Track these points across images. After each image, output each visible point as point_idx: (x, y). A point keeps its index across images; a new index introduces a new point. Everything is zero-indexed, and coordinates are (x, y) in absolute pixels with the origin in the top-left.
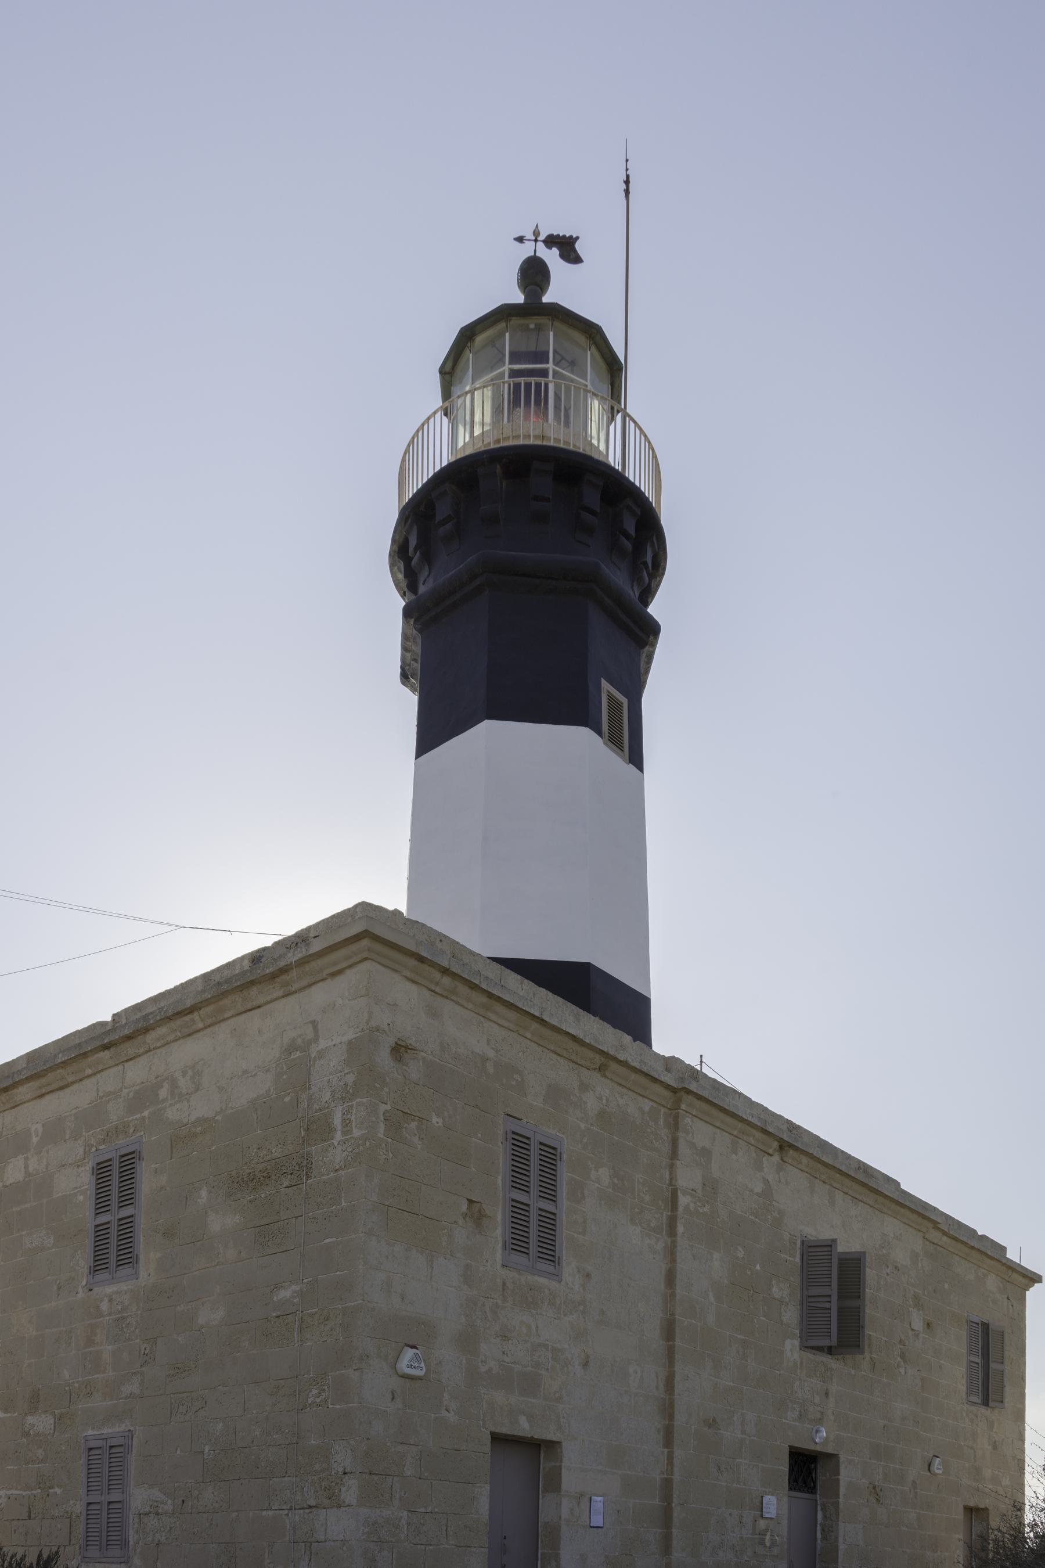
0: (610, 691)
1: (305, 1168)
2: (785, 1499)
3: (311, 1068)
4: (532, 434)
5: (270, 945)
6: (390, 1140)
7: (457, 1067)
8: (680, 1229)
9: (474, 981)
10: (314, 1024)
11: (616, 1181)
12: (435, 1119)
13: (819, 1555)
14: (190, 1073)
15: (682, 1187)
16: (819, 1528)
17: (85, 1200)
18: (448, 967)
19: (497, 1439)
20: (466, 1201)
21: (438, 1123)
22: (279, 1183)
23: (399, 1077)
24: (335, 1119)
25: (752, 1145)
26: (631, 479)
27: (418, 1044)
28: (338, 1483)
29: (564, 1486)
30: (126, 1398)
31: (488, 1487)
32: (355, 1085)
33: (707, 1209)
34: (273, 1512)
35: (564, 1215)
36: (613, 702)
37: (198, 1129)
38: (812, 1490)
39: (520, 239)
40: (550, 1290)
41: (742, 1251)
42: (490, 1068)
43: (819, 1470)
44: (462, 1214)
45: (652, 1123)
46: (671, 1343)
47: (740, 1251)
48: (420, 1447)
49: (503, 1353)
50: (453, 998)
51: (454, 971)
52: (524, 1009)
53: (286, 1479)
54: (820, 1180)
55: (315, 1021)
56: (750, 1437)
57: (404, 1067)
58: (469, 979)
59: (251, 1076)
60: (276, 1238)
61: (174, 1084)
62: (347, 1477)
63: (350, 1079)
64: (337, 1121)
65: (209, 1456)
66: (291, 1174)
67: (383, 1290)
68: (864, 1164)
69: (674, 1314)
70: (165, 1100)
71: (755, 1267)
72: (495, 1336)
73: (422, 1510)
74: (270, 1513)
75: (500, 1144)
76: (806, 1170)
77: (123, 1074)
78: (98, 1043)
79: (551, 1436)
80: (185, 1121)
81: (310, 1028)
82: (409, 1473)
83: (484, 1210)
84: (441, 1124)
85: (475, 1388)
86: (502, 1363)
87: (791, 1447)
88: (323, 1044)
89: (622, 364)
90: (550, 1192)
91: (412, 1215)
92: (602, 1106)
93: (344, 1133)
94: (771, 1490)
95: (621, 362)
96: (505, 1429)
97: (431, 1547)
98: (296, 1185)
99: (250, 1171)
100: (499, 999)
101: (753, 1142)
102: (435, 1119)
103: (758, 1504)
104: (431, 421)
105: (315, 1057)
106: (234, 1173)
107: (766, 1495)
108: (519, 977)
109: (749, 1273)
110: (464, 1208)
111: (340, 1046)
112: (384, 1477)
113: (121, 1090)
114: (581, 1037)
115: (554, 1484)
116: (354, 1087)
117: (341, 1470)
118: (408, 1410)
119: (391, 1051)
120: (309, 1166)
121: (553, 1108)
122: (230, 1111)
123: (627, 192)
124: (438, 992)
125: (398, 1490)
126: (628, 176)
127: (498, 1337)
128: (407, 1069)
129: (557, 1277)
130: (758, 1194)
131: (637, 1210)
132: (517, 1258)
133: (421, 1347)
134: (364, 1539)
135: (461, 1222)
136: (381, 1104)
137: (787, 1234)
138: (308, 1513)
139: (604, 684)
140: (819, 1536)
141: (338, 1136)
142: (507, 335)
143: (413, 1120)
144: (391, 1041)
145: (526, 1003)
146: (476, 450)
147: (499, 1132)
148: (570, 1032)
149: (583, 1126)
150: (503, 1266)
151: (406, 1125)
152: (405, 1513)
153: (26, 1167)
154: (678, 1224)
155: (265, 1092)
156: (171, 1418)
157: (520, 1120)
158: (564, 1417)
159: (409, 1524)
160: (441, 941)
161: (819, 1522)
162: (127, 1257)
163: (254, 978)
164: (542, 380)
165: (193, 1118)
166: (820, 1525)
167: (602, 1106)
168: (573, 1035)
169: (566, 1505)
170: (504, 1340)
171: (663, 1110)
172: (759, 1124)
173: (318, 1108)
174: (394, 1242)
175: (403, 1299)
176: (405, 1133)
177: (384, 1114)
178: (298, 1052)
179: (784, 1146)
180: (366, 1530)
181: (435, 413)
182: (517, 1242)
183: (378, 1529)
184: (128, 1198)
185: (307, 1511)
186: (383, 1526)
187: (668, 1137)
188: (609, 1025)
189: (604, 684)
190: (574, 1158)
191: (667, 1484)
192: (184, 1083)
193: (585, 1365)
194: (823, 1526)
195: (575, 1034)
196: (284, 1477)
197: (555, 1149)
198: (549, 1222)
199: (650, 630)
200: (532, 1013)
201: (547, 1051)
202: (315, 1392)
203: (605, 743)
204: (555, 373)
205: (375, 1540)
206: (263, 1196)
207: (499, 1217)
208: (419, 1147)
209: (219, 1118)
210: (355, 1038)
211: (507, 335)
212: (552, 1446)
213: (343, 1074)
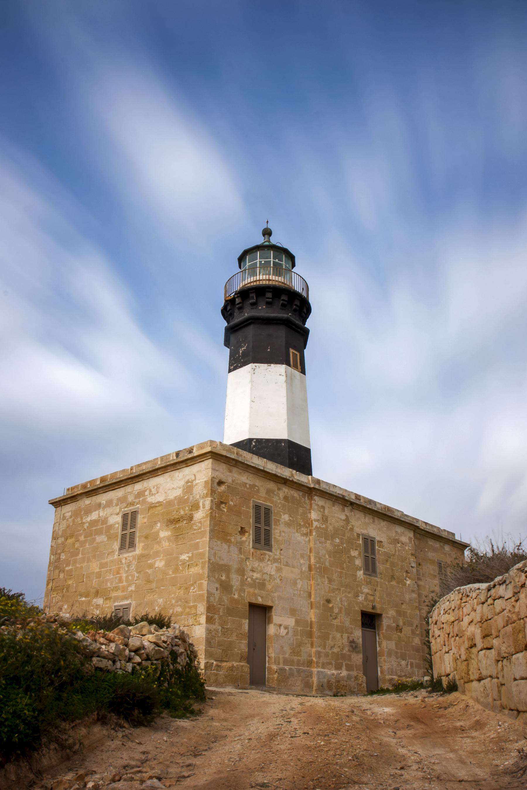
1: (191, 518)
10: (195, 475)
14: (156, 487)
16: (377, 643)
17: (119, 527)
26: (298, 290)
30: (130, 592)
31: (248, 620)
33: (324, 526)
36: (295, 355)
38: (374, 628)
42: (248, 486)
43: (376, 620)
45: (303, 499)
61: (150, 491)
63: (205, 492)
64: (201, 505)
68: (387, 506)
70: (147, 496)
77: (242, 635)
79: (269, 603)
80: (153, 502)
81: (194, 476)
87: (362, 611)
88: (197, 481)
90: (268, 523)
96: (254, 601)
106: (168, 519)
110: (240, 530)
113: (133, 491)
122: (168, 500)
129: (271, 551)
130: (344, 520)
132: (257, 545)
135: (238, 534)
144: (217, 481)
149: (279, 502)
153: (99, 514)
162: (132, 545)
165: (156, 501)
171: (307, 494)
182: (257, 540)
184: (133, 526)
192: (154, 491)
194: (379, 642)
197: (269, 509)
198: (268, 533)
199: (305, 333)
202: (192, 588)
209: (164, 502)
212: (270, 608)
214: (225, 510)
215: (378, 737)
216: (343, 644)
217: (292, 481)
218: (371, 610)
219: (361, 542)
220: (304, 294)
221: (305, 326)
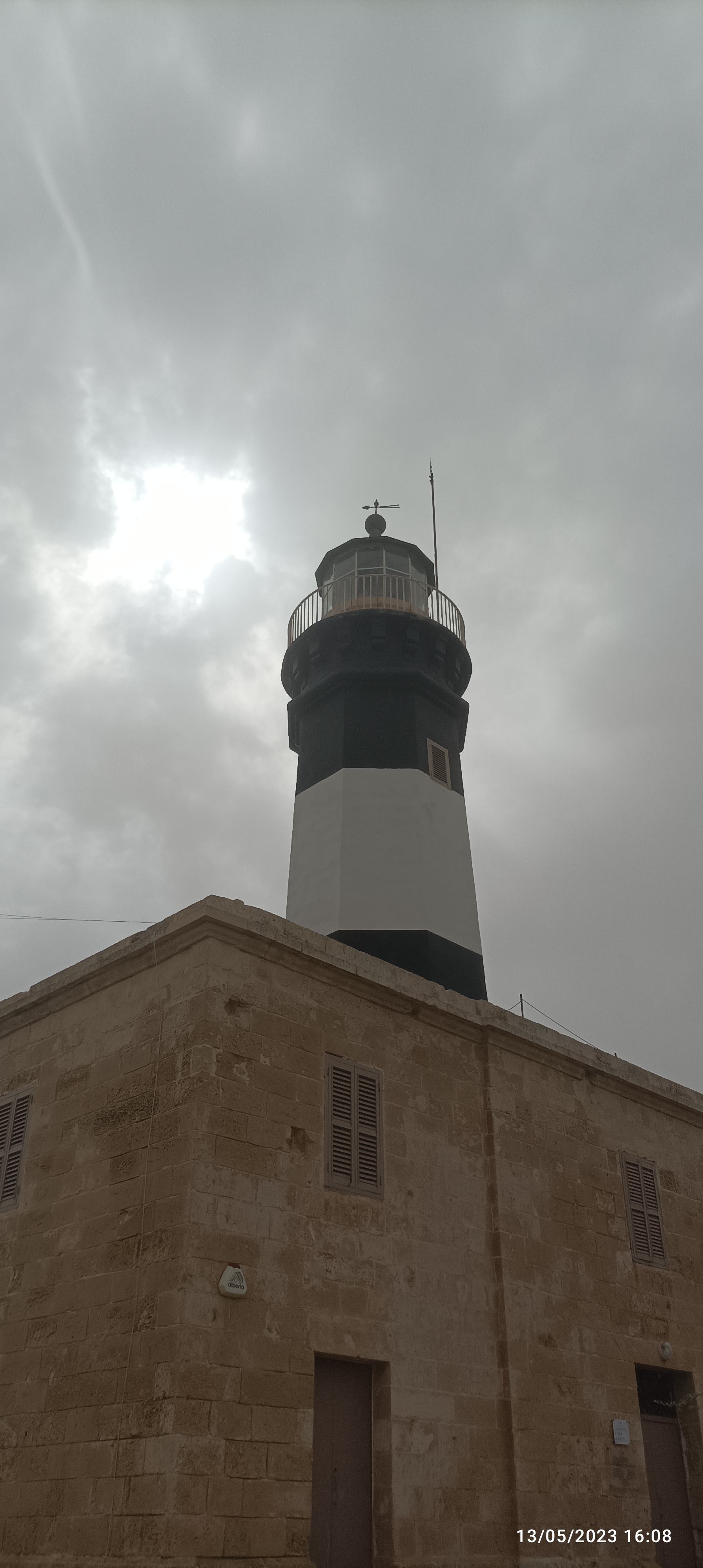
0: (433, 745)
2: (638, 1424)
3: (164, 1022)
4: (364, 604)
5: (145, 929)
6: (221, 1078)
7: (283, 1016)
8: (497, 1148)
9: (297, 949)
11: (433, 1107)
12: (262, 1059)
13: (690, 1489)
15: (497, 1110)
18: (274, 939)
19: (323, 1361)
20: (291, 1128)
21: (265, 1062)
22: (133, 1118)
23: (232, 1026)
24: (178, 1063)
25: (561, 1071)
27: (249, 999)
28: (158, 1409)
29: (394, 1411)
31: (311, 1411)
32: (194, 1034)
34: (100, 1442)
35: (384, 1137)
36: (438, 754)
37: (78, 1075)
39: (367, 508)
40: (372, 1208)
41: (561, 1166)
44: (287, 1140)
46: (498, 1257)
47: (560, 1167)
48: (241, 1369)
49: (327, 1270)
50: (281, 962)
51: (279, 942)
52: (341, 968)
53: (114, 1406)
54: (631, 1100)
55: (168, 985)
56: (590, 1354)
57: (237, 1018)
58: (292, 947)
59: (120, 1030)
60: (126, 1167)
62: (166, 1402)
64: (179, 1065)
65: (53, 1383)
66: (142, 1110)
67: (208, 1212)
68: (675, 1084)
69: (497, 1229)
71: (577, 1181)
72: (318, 1254)
73: (241, 1438)
74: (98, 1444)
75: (323, 1078)
76: (616, 1091)
78: (13, 1009)
79: (377, 1355)
82: (228, 1397)
83: (307, 1135)
84: (268, 1063)
85: (298, 1306)
86: (325, 1280)
89: (412, 564)
90: (369, 1117)
91: (238, 1142)
92: (416, 1043)
93: (183, 1074)
94: (621, 1413)
95: (432, 563)
96: (330, 1349)
97: (250, 1481)
98: (144, 1120)
99: (112, 1109)
100: (318, 962)
101: (561, 1069)
102: (262, 1059)
103: (608, 1429)
104: (307, 601)
105: (167, 1013)
107: (616, 1418)
108: (342, 944)
109: (571, 1187)
110: (289, 1134)
111: (185, 1003)
112: (202, 1401)
114: (392, 988)
115: (384, 1410)
116: (193, 1035)
117: (161, 1394)
118: (229, 1330)
119: (225, 1007)
120: (156, 1102)
121: (371, 1047)
123: (432, 481)
124: (268, 958)
125: (217, 1416)
126: (432, 474)
127: (321, 1255)
128: (239, 1019)
131: (454, 1132)
133: (244, 1266)
134: (178, 1471)
135: (285, 1146)
136: (213, 1049)
137: (606, 1150)
138: (130, 1444)
139: (430, 742)
140: (686, 1466)
141: (179, 1077)
142: (356, 553)
143: (243, 1061)
145: (342, 964)
146: (341, 612)
147: (321, 1068)
148: (382, 984)
150: (326, 1187)
151: (237, 1065)
152: (223, 1442)
154: (495, 1144)
155: (129, 1043)
156: (26, 1344)
157: (341, 1057)
158: (390, 1335)
159: (226, 1454)
160: (274, 920)
161: (684, 1449)
163: (126, 955)
164: (377, 576)
166: (686, 1455)
167: (416, 1043)
168: (385, 987)
169: (396, 1431)
170: (327, 1258)
171: (473, 1045)
172: (563, 1053)
173: (166, 1054)
174: (221, 1167)
175: (228, 1219)
176: (235, 1071)
177: (217, 1056)
178: (155, 1010)
179: (590, 1073)
180: (180, 1462)
181: (312, 594)
183: (194, 1460)
185: (130, 1441)
186: (199, 1457)
187: (480, 1067)
188: (422, 978)
189: (430, 742)
190: (392, 1088)
191: (505, 1406)
193: (410, 1280)
195: (387, 986)
196: (113, 1404)
198: (370, 1145)
200: (348, 971)
201: (364, 1000)
203: (431, 778)
204: (388, 571)
205: (189, 1472)
206: (119, 1130)
207: (322, 1142)
208: (248, 1082)
210: (196, 997)
211: (356, 553)
212: (381, 1367)
213: (185, 1025)
214: (245, 1077)
215: (588, 1449)
216: (594, 1468)
217: (433, 1009)
218: (659, 1364)
219: (619, 1174)
220: (455, 631)
221: (462, 697)
